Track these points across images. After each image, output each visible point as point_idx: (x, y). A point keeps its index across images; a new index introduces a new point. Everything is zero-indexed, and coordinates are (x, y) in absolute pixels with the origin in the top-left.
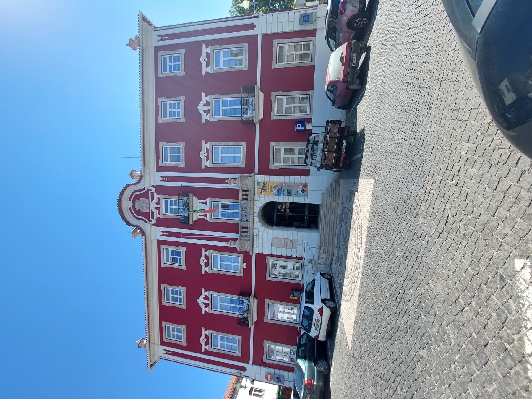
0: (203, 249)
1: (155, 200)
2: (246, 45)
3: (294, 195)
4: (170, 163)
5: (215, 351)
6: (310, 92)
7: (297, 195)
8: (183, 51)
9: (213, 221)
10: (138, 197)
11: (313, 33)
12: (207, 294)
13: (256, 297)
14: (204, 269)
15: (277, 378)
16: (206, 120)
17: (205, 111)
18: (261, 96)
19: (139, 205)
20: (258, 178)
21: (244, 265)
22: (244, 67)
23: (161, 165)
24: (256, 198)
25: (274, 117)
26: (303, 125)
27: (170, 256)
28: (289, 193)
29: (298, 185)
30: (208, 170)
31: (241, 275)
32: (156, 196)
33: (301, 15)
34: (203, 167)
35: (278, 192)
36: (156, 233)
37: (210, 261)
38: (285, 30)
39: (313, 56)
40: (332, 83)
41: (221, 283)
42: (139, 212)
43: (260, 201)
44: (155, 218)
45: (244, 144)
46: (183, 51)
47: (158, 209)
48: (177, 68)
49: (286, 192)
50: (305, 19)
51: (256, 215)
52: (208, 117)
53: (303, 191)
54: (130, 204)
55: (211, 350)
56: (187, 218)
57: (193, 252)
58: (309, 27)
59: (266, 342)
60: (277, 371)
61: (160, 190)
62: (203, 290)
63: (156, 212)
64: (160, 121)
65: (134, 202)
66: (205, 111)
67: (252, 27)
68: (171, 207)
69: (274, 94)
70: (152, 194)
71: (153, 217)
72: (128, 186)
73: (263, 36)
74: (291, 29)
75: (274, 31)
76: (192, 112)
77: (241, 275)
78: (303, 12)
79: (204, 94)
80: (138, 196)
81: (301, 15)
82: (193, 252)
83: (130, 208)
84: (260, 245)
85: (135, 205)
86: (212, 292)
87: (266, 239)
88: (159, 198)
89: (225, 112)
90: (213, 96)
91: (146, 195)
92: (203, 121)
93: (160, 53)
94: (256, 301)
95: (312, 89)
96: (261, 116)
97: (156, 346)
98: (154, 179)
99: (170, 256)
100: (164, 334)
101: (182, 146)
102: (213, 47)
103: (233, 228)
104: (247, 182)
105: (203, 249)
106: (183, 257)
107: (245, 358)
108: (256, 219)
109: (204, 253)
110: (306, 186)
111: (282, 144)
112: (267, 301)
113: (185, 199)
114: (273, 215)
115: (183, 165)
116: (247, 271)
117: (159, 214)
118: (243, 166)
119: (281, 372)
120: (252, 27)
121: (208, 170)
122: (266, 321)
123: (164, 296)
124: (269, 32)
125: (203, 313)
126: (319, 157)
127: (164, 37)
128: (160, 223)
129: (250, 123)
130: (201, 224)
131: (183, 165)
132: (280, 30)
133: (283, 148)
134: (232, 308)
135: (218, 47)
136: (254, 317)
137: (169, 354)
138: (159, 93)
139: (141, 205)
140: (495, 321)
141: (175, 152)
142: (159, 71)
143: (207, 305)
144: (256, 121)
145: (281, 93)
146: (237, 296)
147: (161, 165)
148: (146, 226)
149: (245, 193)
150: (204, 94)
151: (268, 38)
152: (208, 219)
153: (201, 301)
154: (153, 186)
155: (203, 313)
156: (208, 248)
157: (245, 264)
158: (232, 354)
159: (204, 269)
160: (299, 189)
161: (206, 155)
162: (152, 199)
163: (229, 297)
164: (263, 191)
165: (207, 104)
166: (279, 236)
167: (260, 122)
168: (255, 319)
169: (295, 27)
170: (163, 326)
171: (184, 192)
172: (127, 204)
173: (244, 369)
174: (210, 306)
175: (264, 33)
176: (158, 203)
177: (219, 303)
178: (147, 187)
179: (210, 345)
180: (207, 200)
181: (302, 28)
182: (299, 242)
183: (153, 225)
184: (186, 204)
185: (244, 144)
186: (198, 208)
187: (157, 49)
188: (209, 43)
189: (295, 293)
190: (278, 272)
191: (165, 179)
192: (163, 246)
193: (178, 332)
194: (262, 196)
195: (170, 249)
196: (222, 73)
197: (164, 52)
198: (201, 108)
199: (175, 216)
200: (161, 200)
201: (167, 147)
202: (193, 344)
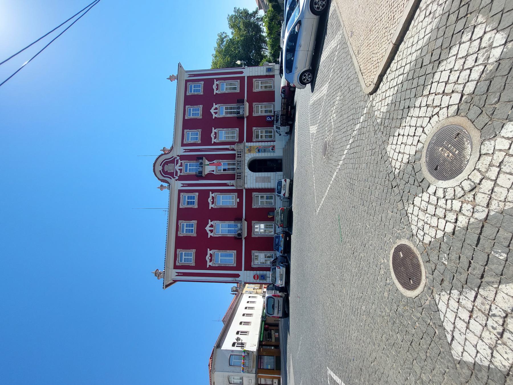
0: (211, 192)
1: (179, 164)
2: (239, 81)
3: (267, 152)
4: (183, 262)
5: (217, 265)
6: (273, 103)
7: (269, 151)
8: (203, 83)
9: (218, 174)
10: (167, 163)
11: (273, 76)
12: (212, 223)
13: (245, 220)
14: (211, 206)
15: (262, 276)
16: (211, 236)
17: (210, 230)
18: (247, 105)
19: (166, 168)
20: (247, 144)
21: (238, 200)
22: (238, 91)
23: (177, 264)
24: (246, 155)
25: (255, 115)
26: (271, 118)
27: (187, 200)
28: (265, 151)
29: (269, 147)
30: (215, 144)
31: (236, 207)
32: (180, 161)
33: (266, 280)
34: (213, 142)
35: (259, 151)
36: (178, 185)
37: (215, 200)
38: (259, 74)
39: (274, 87)
40: (283, 88)
41: (223, 214)
42: (166, 173)
43: (248, 157)
44: (178, 175)
45: (238, 129)
46: (203, 83)
47: (181, 170)
48: (199, 91)
49: (263, 151)
50: (269, 70)
51: (246, 164)
52: (216, 116)
53: (272, 149)
54: (161, 168)
55: (214, 265)
56: (201, 172)
57: (204, 196)
58: (271, 74)
59: (253, 252)
60: (261, 272)
61: (182, 157)
62: (214, 104)
63: (179, 171)
64: (181, 207)
65: (163, 167)
66: (210, 230)
67: (242, 73)
68: (191, 168)
69: (254, 104)
70: (177, 161)
71: (176, 175)
72: (158, 178)
73: (248, 77)
74: (262, 74)
75: (254, 75)
76: (206, 112)
77: (236, 207)
78: (268, 67)
79: (210, 220)
80: (166, 163)
81: (266, 280)
82: (204, 196)
83: (160, 171)
84: (249, 183)
85: (165, 168)
86: (215, 222)
87: (252, 180)
88: (181, 163)
89: (227, 113)
90: (219, 105)
91: (173, 162)
92: (209, 237)
93: (188, 83)
94: (246, 223)
95: (274, 101)
96: (247, 114)
97: (170, 270)
98: (180, 151)
99: (187, 200)
100: (178, 259)
101: (194, 222)
102: (220, 81)
103: (232, 177)
104: (241, 146)
105: (211, 192)
106: (196, 200)
107: (238, 267)
108: (246, 167)
109: (211, 195)
110: (274, 147)
111: (259, 128)
112: (253, 222)
113: (201, 161)
114: (256, 166)
115: (200, 142)
116: (240, 204)
117: (181, 172)
118: (235, 265)
119: (265, 272)
120: (242, 73)
121: (215, 144)
122: (253, 236)
123: (180, 229)
124: (251, 75)
125: (214, 118)
126: (279, 121)
127: (191, 76)
128: (181, 178)
129: (242, 118)
130: (210, 176)
131: (200, 142)
132: (256, 75)
133: (260, 196)
134: (229, 231)
135: (223, 81)
136: (245, 234)
137: (180, 275)
138: (186, 103)
139: (169, 168)
140: (370, 85)
141: (194, 136)
142: (187, 92)
143: (216, 113)
144: (245, 116)
145: (258, 103)
146: (233, 222)
147: (177, 264)
148: (172, 181)
149: (239, 153)
150: (210, 220)
151: (250, 78)
152: (214, 173)
153: (208, 228)
154: (178, 156)
155: (214, 118)
156: (213, 191)
157: (238, 199)
158: (230, 265)
159: (210, 234)
160: (270, 149)
161: (210, 258)
162: (177, 163)
163: (227, 223)
164: (250, 151)
165: (216, 109)
166: (260, 176)
167: (247, 117)
168: (246, 235)
169: (265, 74)
170: (178, 253)
171: (200, 157)
172: (159, 168)
173: (238, 276)
174: (214, 231)
175: (248, 75)
176: (181, 166)
177: (220, 228)
178: (175, 156)
179: (213, 261)
180: (215, 161)
181: (268, 74)
182: (272, 178)
183: (176, 180)
184: (201, 163)
185: (238, 129)
186: (208, 169)
187: (187, 81)
188: (217, 79)
189: (271, 213)
190: (260, 202)
191: (184, 185)
192: (182, 194)
193: (189, 256)
194: (249, 154)
195: (187, 195)
196: (225, 94)
197: (191, 83)
198: (212, 111)
199: (194, 173)
200: (183, 164)
201: (184, 224)
202: (200, 263)
